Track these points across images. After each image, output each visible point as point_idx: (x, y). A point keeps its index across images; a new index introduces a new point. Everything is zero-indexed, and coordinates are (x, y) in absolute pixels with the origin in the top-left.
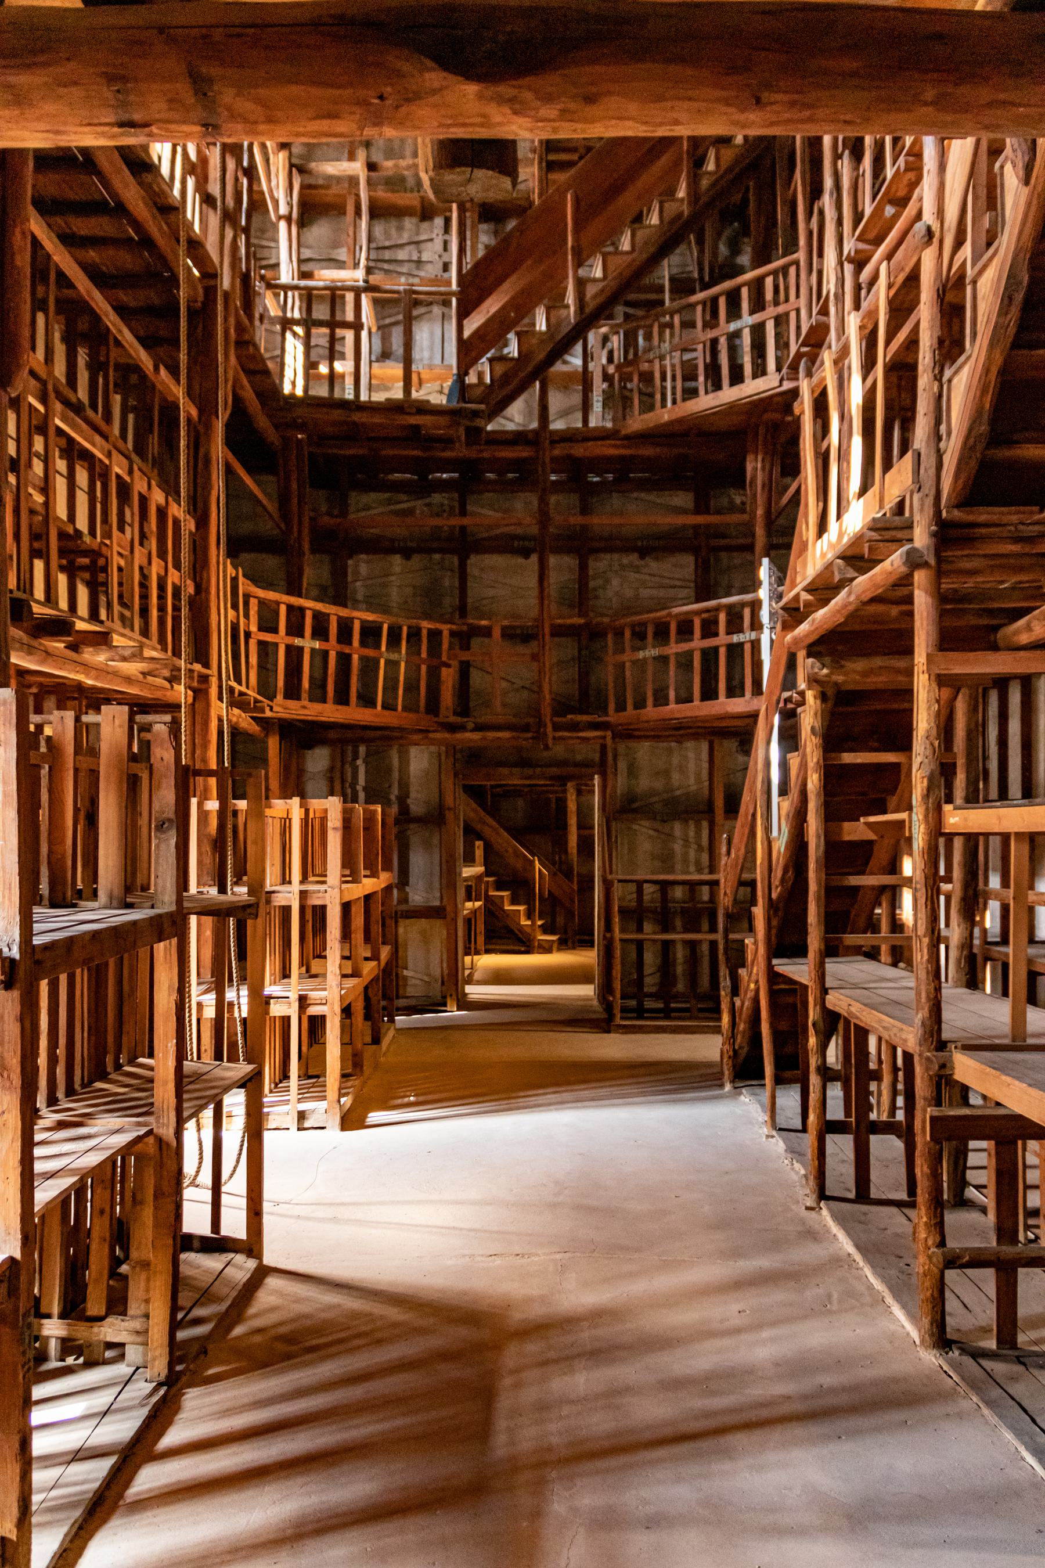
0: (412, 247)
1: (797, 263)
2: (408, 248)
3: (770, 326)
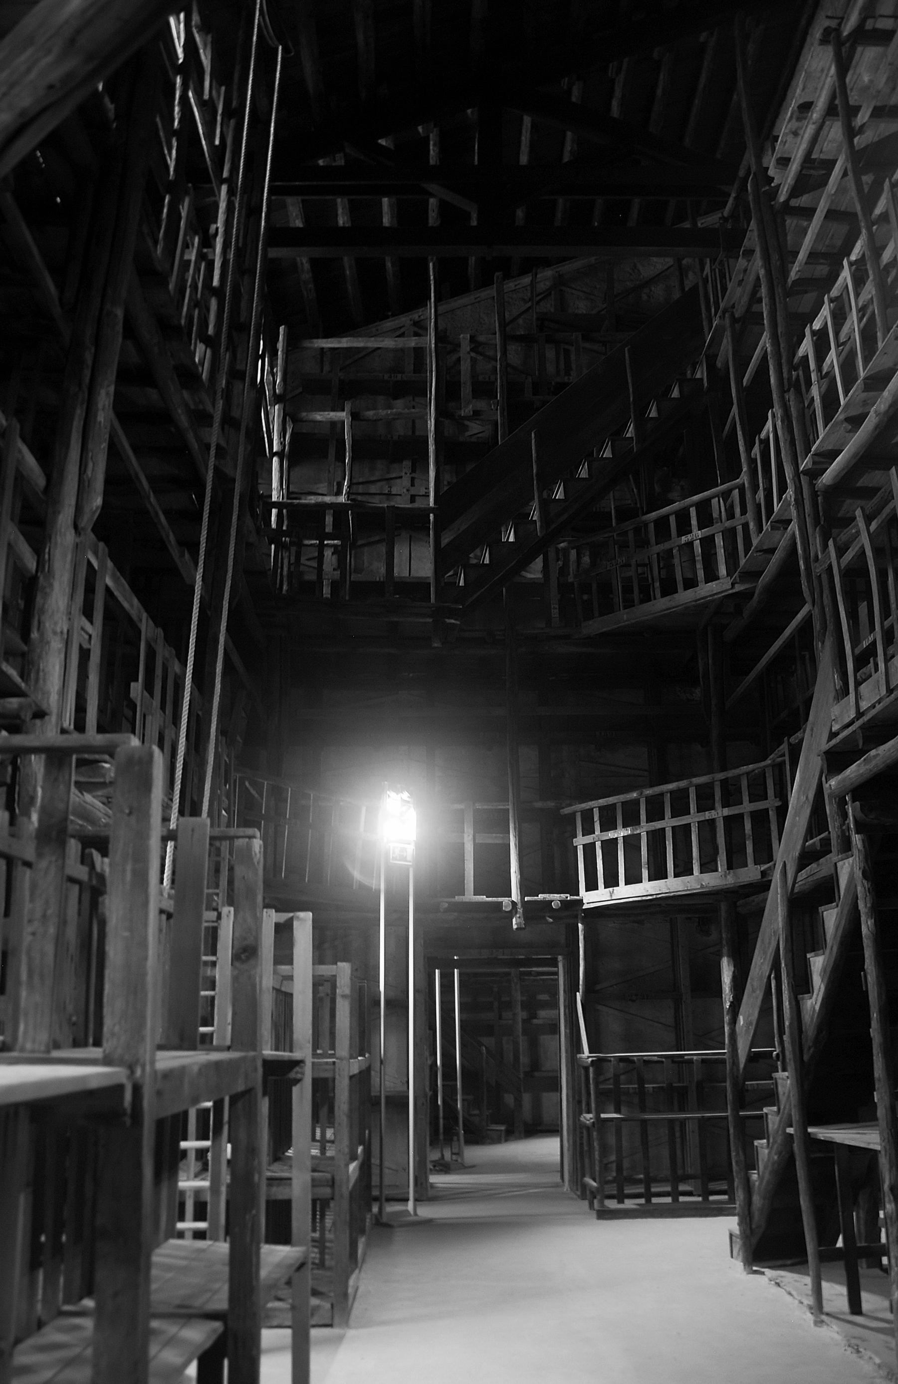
0: (384, 483)
1: (742, 488)
2: (379, 484)
3: (719, 541)
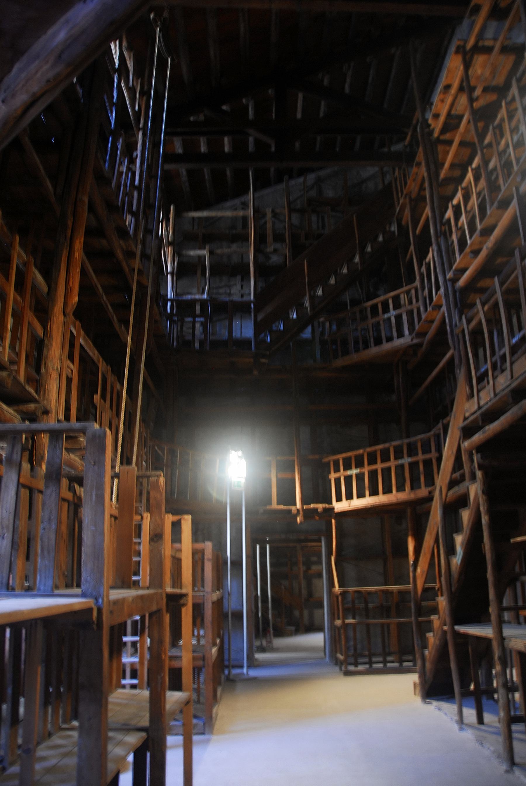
3: (404, 317)
